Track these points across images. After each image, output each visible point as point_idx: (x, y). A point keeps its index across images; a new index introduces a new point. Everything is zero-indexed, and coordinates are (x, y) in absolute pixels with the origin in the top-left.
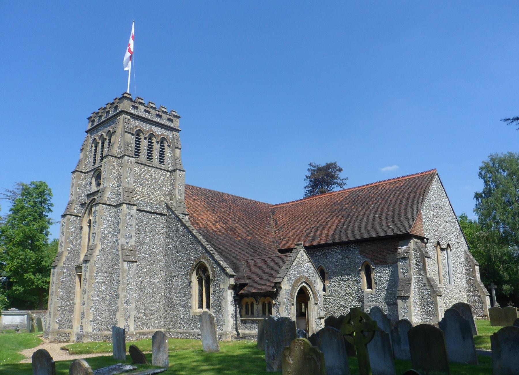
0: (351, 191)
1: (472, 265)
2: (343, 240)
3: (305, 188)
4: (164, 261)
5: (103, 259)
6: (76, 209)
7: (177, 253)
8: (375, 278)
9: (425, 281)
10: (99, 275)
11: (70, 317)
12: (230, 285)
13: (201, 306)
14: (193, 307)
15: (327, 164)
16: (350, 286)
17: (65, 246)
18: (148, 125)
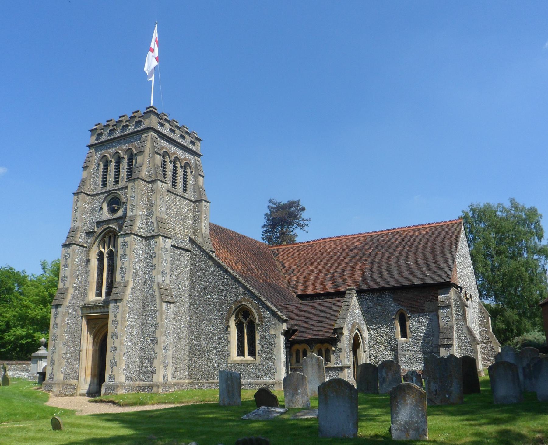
0: (368, 236)
1: (486, 316)
2: (375, 287)
3: (263, 227)
4: (188, 303)
5: (135, 298)
6: (80, 238)
7: (207, 294)
8: (411, 327)
9: (465, 330)
10: (131, 316)
11: (75, 366)
12: (284, 330)
13: (241, 353)
14: (232, 355)
15: (289, 201)
16: (382, 335)
17: (70, 281)
18: (172, 146)
